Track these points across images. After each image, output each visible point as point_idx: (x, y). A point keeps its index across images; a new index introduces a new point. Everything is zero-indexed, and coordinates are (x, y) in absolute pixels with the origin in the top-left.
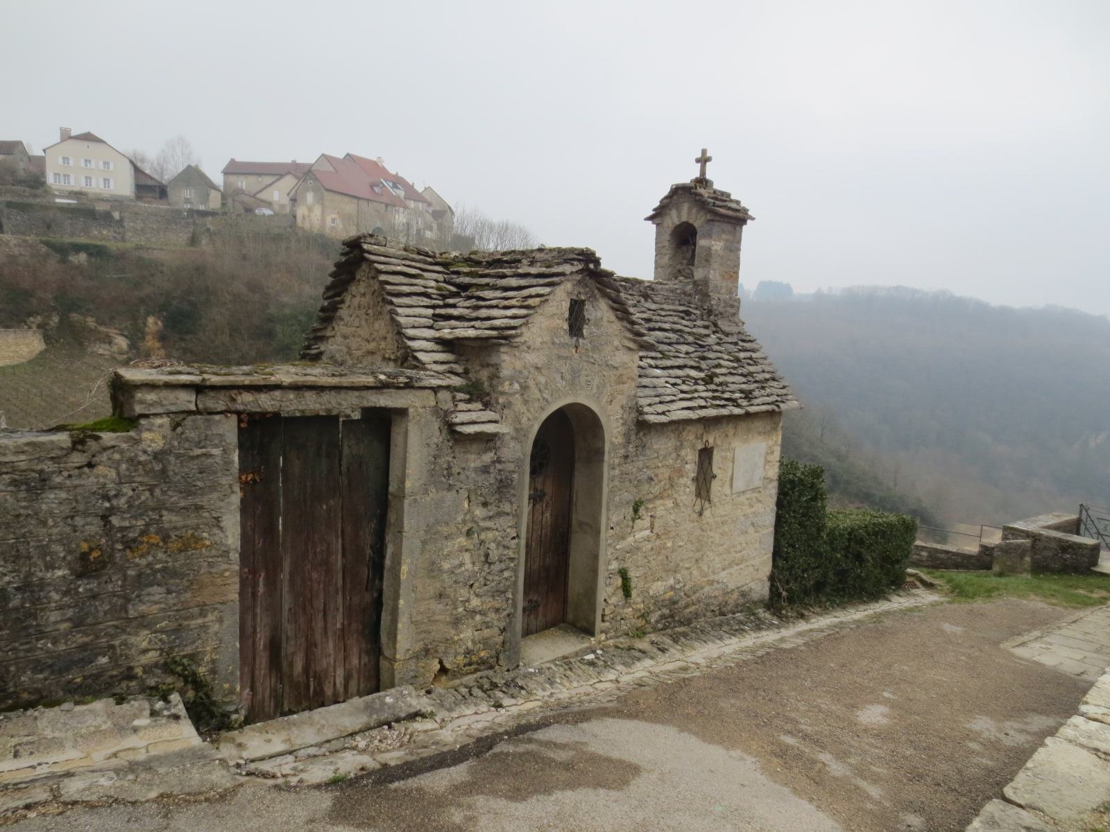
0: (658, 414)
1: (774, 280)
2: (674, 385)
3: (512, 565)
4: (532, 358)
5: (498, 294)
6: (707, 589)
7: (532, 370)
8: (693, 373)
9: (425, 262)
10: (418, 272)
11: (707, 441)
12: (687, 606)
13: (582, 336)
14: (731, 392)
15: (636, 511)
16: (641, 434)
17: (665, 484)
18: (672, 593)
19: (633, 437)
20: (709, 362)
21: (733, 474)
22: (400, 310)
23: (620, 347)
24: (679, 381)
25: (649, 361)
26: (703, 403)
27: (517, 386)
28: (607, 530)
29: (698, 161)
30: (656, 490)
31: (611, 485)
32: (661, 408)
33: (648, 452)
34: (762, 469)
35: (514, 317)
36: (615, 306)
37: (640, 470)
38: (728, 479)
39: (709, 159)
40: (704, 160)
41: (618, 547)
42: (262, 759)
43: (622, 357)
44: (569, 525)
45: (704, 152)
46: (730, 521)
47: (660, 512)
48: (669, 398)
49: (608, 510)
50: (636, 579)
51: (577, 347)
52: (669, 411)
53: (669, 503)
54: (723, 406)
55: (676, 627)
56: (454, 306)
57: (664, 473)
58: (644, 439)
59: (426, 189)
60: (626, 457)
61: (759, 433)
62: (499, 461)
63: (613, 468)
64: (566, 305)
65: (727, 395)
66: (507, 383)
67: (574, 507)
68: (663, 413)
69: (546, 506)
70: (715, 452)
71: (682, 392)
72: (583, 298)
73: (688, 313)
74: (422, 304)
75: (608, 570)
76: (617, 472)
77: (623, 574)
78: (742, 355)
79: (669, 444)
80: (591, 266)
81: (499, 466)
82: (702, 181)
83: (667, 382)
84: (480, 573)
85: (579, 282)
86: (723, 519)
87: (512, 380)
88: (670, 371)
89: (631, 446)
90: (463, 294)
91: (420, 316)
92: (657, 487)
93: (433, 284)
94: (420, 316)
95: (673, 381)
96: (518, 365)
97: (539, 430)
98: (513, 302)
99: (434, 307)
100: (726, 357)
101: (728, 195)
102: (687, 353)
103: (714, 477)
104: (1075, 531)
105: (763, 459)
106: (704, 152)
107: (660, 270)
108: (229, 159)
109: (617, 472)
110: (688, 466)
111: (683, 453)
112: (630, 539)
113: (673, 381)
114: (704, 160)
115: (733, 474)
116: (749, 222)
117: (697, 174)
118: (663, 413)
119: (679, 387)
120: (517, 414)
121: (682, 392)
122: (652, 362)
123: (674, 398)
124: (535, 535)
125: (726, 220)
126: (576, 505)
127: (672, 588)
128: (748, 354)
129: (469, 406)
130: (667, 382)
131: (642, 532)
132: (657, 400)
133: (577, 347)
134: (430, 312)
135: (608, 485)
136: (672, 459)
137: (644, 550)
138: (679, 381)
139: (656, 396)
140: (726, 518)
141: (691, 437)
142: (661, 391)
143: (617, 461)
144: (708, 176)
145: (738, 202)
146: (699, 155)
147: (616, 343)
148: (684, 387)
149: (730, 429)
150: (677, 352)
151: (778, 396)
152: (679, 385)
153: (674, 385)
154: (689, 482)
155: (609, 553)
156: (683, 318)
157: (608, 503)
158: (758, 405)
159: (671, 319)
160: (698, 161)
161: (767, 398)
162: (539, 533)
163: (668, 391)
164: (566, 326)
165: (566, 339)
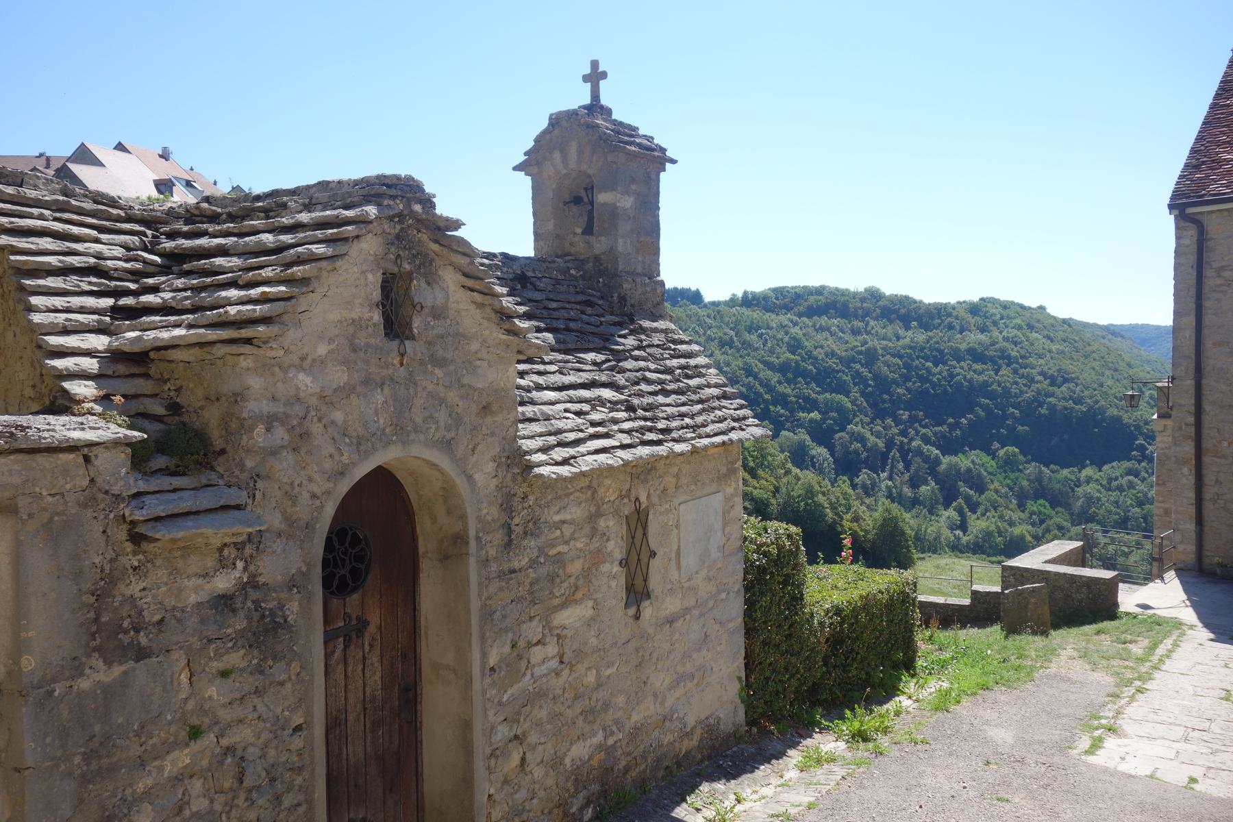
0: (557, 464)
1: (679, 287)
2: (579, 414)
3: (299, 780)
5: (235, 262)
8: (607, 393)
9: (110, 218)
10: (94, 233)
11: (637, 499)
13: (412, 337)
14: (667, 419)
20: (628, 374)
21: (679, 547)
22: (35, 300)
24: (586, 407)
25: (535, 378)
26: (626, 440)
28: (483, 674)
29: (586, 78)
32: (559, 454)
34: (719, 534)
35: (264, 299)
36: (470, 283)
38: (673, 556)
39: (604, 75)
40: (595, 76)
42: (590, 371)
44: (417, 671)
45: (595, 64)
48: (572, 436)
49: (483, 638)
52: (575, 457)
54: (659, 443)
56: (155, 290)
59: (233, 188)
62: (253, 583)
64: (374, 280)
65: (661, 425)
66: (260, 429)
67: (423, 637)
68: (565, 462)
69: (371, 646)
71: (594, 424)
72: (407, 266)
73: (589, 304)
74: (86, 287)
78: (675, 362)
80: (418, 208)
82: (595, 107)
83: (566, 411)
84: (228, 813)
88: (571, 392)
90: (175, 269)
91: (82, 310)
92: (565, 585)
93: (118, 252)
94: (82, 310)
95: (576, 407)
97: (337, 513)
98: (267, 273)
99: (117, 293)
100: (653, 366)
101: (635, 129)
102: (594, 363)
103: (653, 554)
104: (1080, 562)
105: (720, 518)
106: (595, 64)
107: (542, 243)
111: (602, 523)
113: (576, 407)
114: (595, 76)
115: (679, 547)
116: (668, 165)
117: (587, 100)
118: (565, 462)
119: (588, 417)
120: (288, 488)
121: (594, 424)
122: (541, 380)
123: (581, 435)
124: (352, 701)
125: (419, 750)
126: (426, 634)
127: (600, 747)
128: (683, 361)
129: (177, 482)
130: (566, 411)
132: (552, 440)
134: (109, 302)
135: (480, 596)
138: (586, 407)
139: (550, 434)
142: (560, 424)
144: (605, 100)
145: (650, 139)
146: (588, 71)
148: (596, 416)
150: (578, 362)
151: (734, 420)
152: (587, 413)
153: (579, 414)
154: (616, 568)
156: (583, 313)
157: (481, 627)
158: (708, 436)
159: (564, 313)
160: (586, 78)
161: (720, 425)
162: (361, 694)
163: (569, 424)
164: (377, 317)
165: (379, 339)
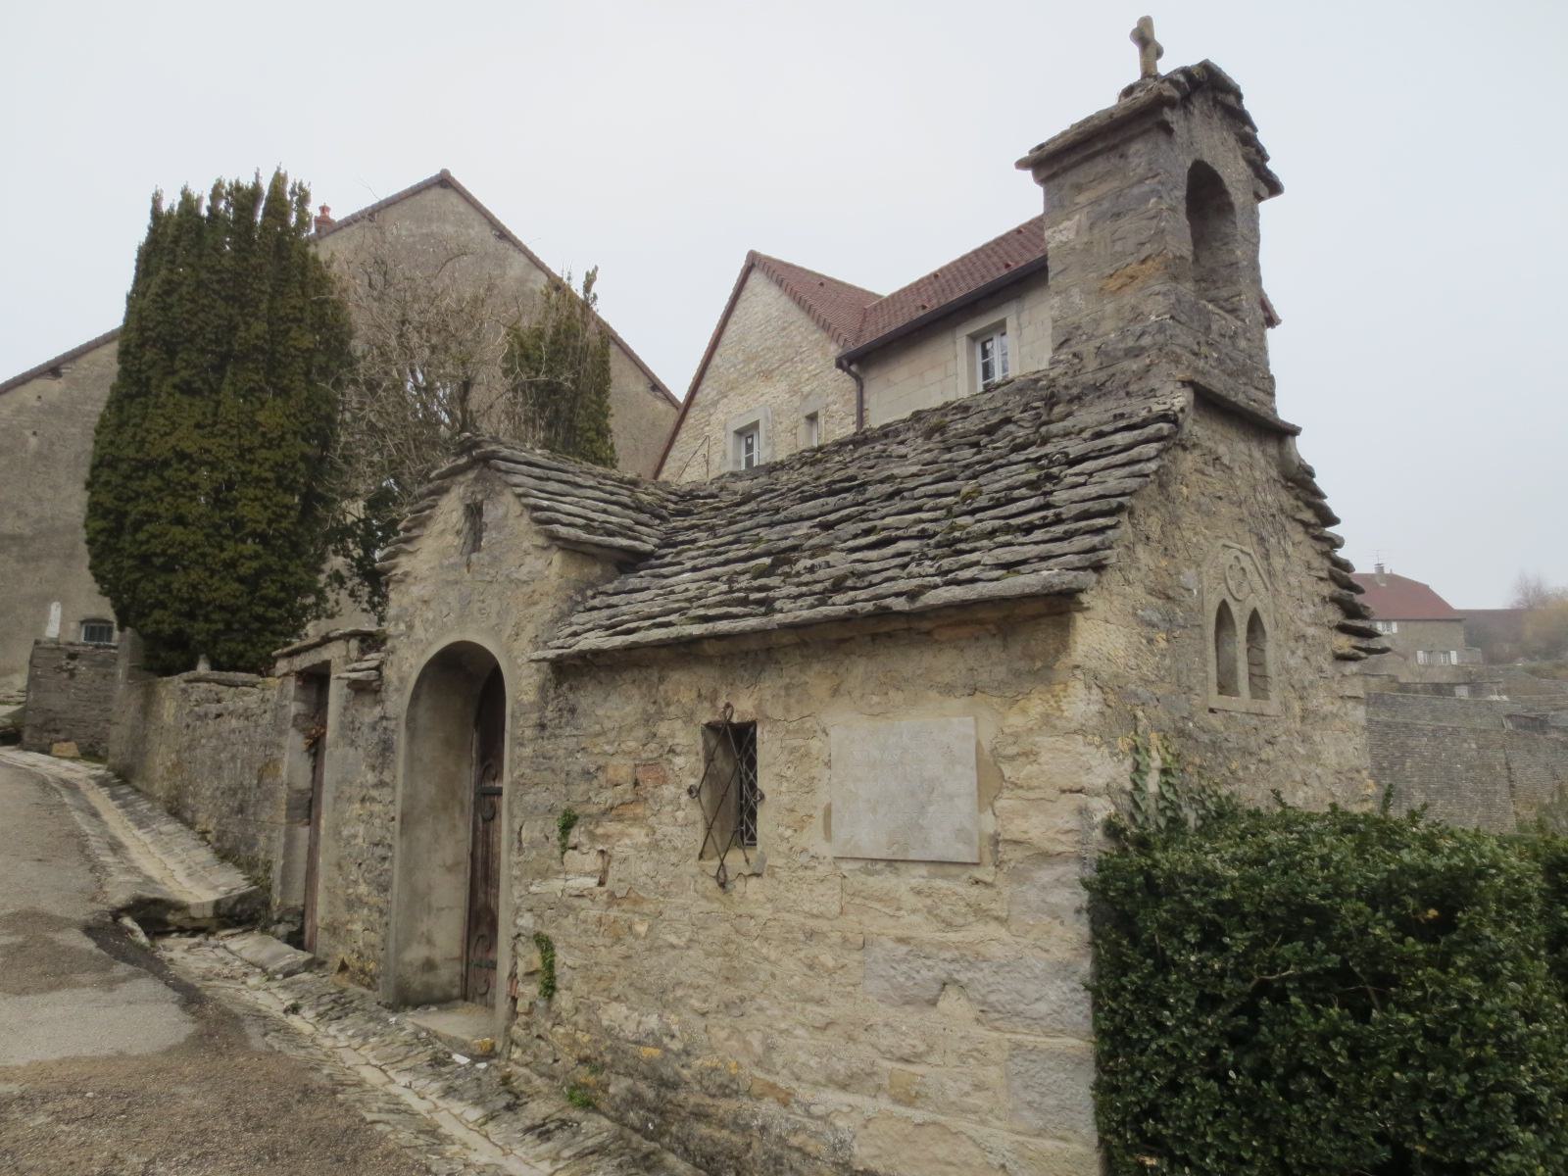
4: (416, 591)
6: (768, 1107)
7: (419, 605)
12: (701, 1115)
15: (567, 827)
16: (566, 686)
17: (625, 792)
18: (656, 1053)
19: (551, 693)
23: (531, 549)
27: (402, 627)
30: (608, 797)
31: (516, 774)
33: (584, 722)
37: (571, 753)
41: (533, 889)
43: (534, 563)
46: (835, 937)
47: (622, 848)
49: (512, 816)
50: (569, 974)
51: (468, 565)
53: (639, 835)
55: (673, 1151)
57: (621, 768)
58: (571, 696)
60: (542, 726)
61: (948, 690)
63: (522, 745)
70: (762, 734)
75: (516, 925)
76: (528, 751)
77: (544, 944)
79: (628, 709)
81: (385, 723)
85: (476, 479)
86: (811, 923)
87: (398, 619)
89: (550, 708)
96: (406, 601)
108: (1297, 424)
109: (528, 751)
110: (679, 761)
112: (557, 884)
125: (1074, 158)
131: (579, 873)
133: (468, 565)
136: (636, 739)
137: (582, 915)
140: (823, 925)
141: (687, 697)
143: (529, 733)
147: (526, 544)
149: (816, 678)
155: (516, 894)
